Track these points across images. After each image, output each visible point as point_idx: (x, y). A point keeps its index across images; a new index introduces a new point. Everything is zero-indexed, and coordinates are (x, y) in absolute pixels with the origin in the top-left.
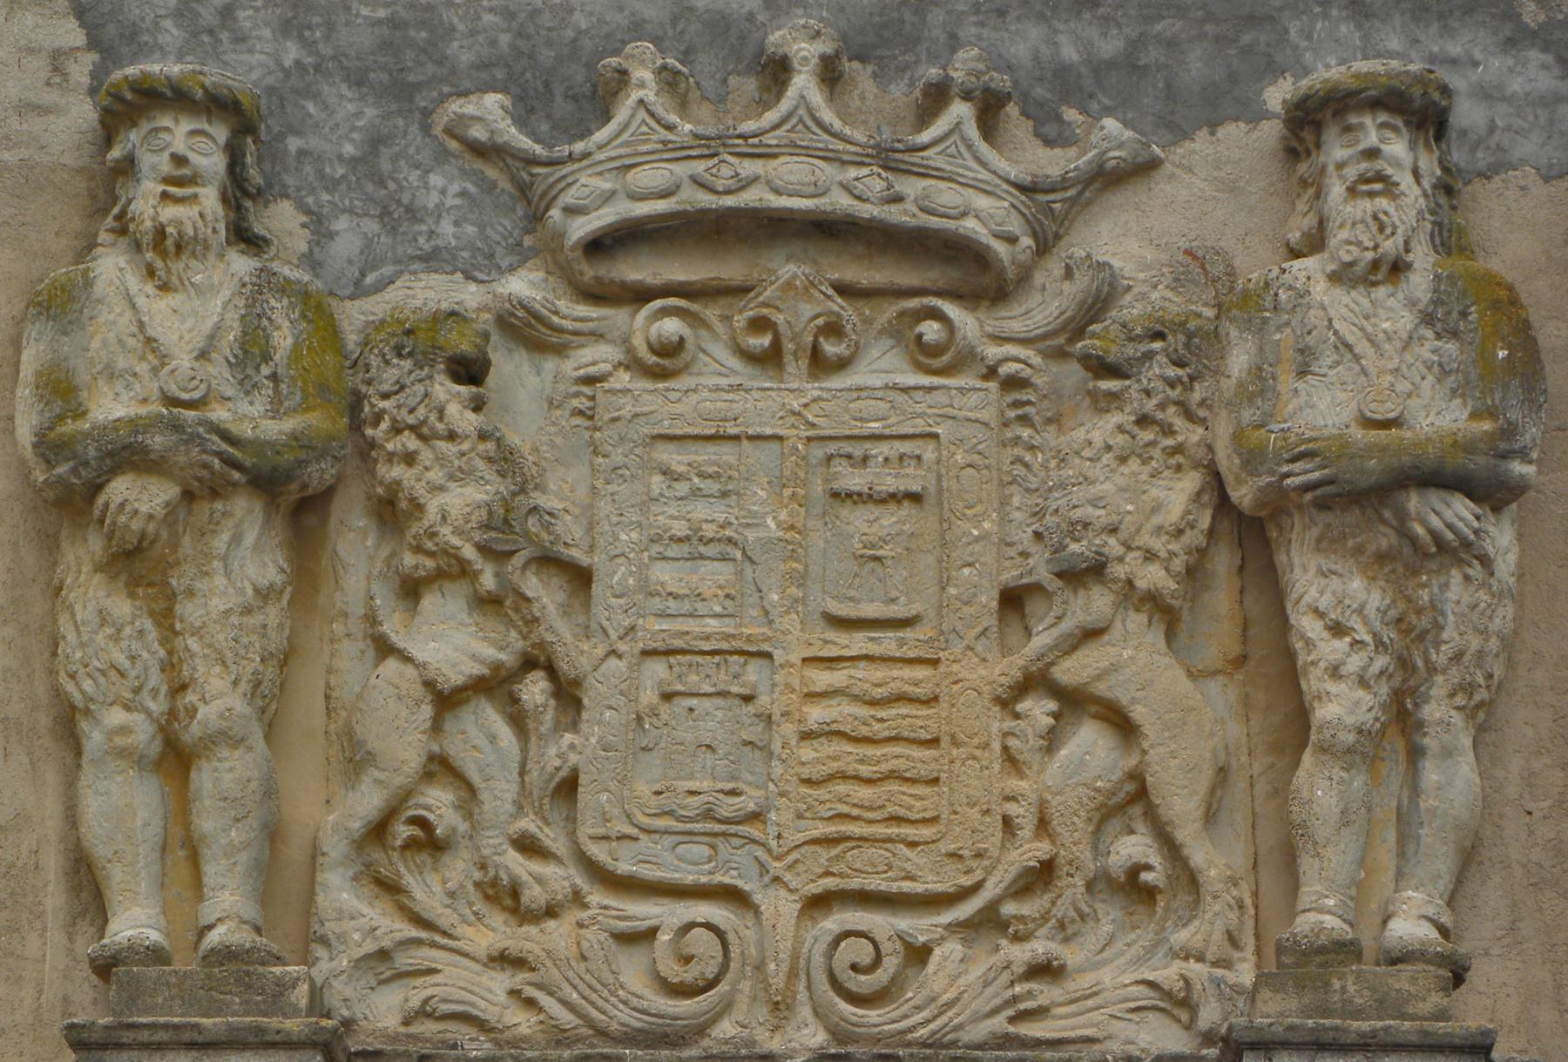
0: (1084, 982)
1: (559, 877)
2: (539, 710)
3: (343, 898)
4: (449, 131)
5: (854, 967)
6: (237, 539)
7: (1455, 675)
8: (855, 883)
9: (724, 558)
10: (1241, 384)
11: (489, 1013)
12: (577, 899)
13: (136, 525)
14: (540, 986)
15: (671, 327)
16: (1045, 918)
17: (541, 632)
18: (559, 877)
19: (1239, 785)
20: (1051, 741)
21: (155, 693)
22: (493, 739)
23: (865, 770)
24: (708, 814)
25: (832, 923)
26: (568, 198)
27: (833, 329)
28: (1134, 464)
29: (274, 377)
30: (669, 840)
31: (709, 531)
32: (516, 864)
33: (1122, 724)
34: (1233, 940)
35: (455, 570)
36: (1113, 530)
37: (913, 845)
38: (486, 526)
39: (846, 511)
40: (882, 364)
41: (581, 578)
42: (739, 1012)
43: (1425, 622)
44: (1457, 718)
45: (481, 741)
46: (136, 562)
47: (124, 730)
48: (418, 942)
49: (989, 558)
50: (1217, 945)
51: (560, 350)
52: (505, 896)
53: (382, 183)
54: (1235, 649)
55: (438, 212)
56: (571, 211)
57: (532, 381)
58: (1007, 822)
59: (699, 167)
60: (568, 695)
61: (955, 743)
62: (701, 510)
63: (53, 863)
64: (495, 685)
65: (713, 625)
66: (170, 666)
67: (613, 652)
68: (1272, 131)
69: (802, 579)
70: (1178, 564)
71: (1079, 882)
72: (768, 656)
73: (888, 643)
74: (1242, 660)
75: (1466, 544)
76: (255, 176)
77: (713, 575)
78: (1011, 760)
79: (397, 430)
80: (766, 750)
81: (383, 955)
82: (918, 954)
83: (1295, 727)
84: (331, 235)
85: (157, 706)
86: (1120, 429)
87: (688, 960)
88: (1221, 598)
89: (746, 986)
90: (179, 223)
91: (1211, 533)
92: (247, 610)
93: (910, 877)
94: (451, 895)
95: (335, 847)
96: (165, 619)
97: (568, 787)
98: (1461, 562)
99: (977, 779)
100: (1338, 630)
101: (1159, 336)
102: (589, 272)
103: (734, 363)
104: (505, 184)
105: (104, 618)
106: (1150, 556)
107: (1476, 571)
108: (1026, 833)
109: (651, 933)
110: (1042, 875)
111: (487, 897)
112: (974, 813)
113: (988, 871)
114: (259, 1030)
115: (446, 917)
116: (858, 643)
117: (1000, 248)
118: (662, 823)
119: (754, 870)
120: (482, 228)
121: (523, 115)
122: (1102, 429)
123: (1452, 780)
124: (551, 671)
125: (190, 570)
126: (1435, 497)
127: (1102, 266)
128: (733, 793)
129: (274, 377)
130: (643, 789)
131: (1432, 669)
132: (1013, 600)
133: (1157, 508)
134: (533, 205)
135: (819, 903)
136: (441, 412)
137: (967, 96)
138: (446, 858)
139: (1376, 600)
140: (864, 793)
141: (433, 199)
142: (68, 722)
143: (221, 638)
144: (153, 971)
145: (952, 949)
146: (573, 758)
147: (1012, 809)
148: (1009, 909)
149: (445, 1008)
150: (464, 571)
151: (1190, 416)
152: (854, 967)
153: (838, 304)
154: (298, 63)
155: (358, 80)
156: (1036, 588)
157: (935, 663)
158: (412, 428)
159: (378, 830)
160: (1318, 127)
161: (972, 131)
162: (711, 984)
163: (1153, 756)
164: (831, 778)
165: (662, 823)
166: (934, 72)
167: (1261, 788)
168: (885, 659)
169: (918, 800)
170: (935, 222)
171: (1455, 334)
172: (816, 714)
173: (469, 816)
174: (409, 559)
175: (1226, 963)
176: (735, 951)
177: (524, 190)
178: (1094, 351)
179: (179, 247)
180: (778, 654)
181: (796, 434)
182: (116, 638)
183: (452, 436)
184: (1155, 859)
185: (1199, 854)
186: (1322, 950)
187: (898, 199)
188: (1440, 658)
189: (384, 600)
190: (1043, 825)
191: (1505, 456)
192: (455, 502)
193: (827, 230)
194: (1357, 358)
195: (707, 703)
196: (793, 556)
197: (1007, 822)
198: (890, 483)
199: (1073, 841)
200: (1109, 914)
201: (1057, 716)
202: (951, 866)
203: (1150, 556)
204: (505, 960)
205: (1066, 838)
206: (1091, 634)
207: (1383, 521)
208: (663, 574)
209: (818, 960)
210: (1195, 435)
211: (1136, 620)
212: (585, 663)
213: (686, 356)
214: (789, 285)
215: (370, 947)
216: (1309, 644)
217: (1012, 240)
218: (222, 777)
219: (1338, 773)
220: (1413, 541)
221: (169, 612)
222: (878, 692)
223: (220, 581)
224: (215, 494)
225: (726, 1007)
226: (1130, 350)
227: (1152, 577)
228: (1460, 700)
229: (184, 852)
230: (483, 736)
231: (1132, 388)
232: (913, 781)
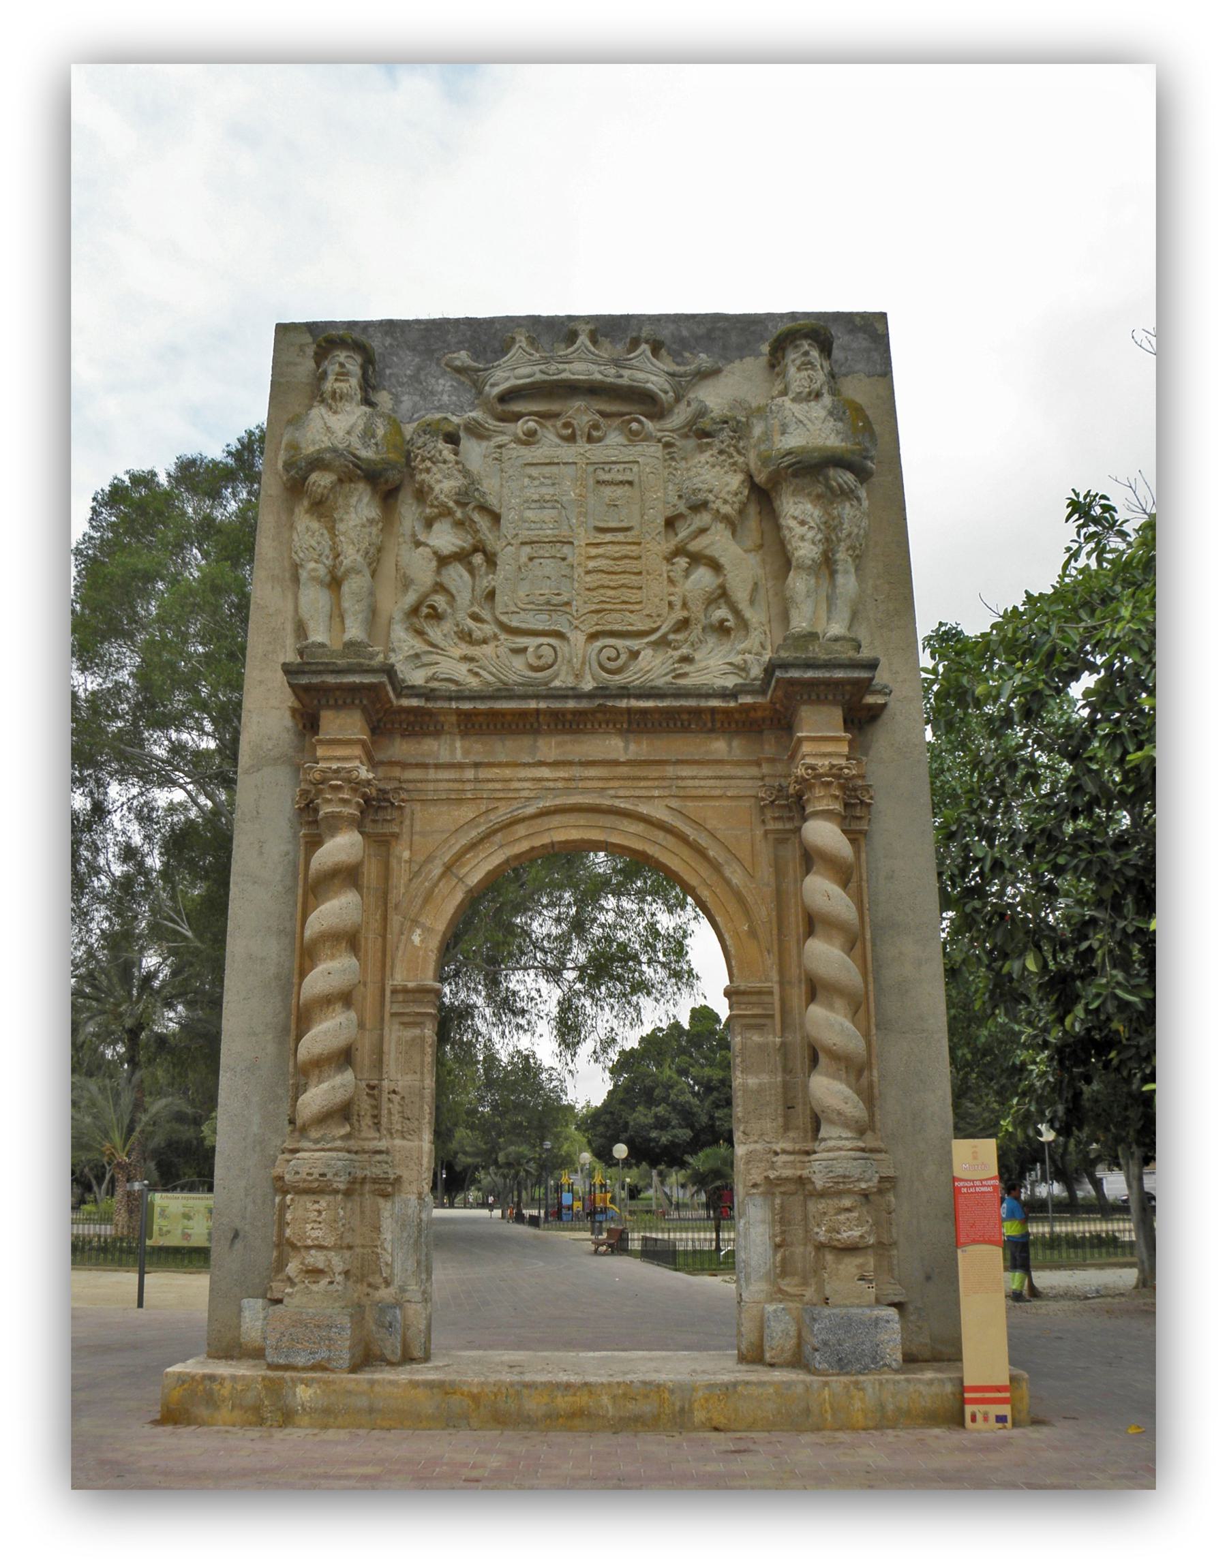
0: (703, 664)
1: (489, 629)
2: (480, 566)
3: (400, 634)
4: (447, 365)
5: (609, 659)
6: (360, 500)
7: (848, 542)
8: (608, 628)
9: (554, 508)
10: (759, 438)
11: (460, 678)
12: (496, 637)
13: (319, 490)
14: (480, 667)
15: (532, 424)
16: (686, 641)
17: (481, 535)
18: (489, 629)
19: (762, 591)
20: (687, 573)
21: (328, 558)
22: (461, 577)
23: (612, 584)
24: (548, 603)
25: (599, 644)
26: (492, 381)
27: (596, 427)
28: (718, 468)
29: (376, 444)
30: (532, 613)
31: (547, 497)
32: (471, 623)
33: (716, 567)
34: (763, 646)
35: (446, 513)
36: (711, 491)
37: (632, 612)
38: (457, 494)
39: (602, 488)
40: (615, 438)
41: (496, 518)
42: (561, 677)
43: (836, 522)
44: (849, 559)
45: (457, 578)
46: (321, 507)
47: (314, 570)
48: (431, 653)
49: (661, 506)
50: (756, 648)
51: (488, 438)
52: (467, 637)
53: (421, 383)
54: (759, 542)
55: (442, 393)
56: (493, 385)
57: (478, 449)
58: (670, 604)
59: (543, 367)
60: (491, 561)
61: (648, 573)
62: (544, 490)
63: (290, 627)
64: (462, 557)
65: (549, 532)
66: (333, 548)
67: (509, 544)
68: (763, 360)
69: (585, 514)
70: (736, 506)
71: (699, 627)
72: (572, 543)
73: (620, 537)
74: (761, 546)
75: (852, 491)
76: (373, 381)
77: (548, 514)
78: (671, 581)
79: (423, 461)
80: (571, 578)
81: (417, 656)
82: (634, 655)
83: (785, 562)
84: (401, 402)
85: (329, 562)
86: (712, 456)
87: (540, 657)
88: (753, 522)
89: (564, 668)
90: (341, 389)
91: (748, 498)
92: (363, 526)
93: (631, 625)
94: (445, 635)
95: (398, 616)
96: (332, 530)
97: (491, 595)
98: (849, 499)
99: (656, 588)
100: (803, 523)
101: (726, 422)
102: (499, 408)
103: (558, 441)
104: (467, 382)
105: (308, 529)
106: (725, 502)
107: (855, 503)
108: (678, 607)
109: (525, 650)
110: (684, 624)
111: (459, 638)
112: (657, 600)
113: (663, 622)
114: (361, 665)
115: (442, 644)
116: (608, 537)
117: (662, 395)
118: (529, 607)
119: (567, 624)
120: (459, 397)
121: (476, 356)
122: (705, 457)
123: (847, 583)
124: (485, 552)
125: (341, 511)
126: (840, 471)
127: (702, 401)
128: (558, 594)
129: (376, 444)
130: (521, 594)
131: (839, 540)
132: (670, 523)
133: (727, 485)
134: (478, 388)
135: (593, 637)
136: (441, 452)
137: (647, 342)
138: (443, 623)
139: (817, 513)
140: (611, 593)
141: (440, 388)
142: (296, 567)
143: (353, 535)
144: (321, 650)
145: (647, 654)
146: (493, 583)
147: (672, 598)
148: (671, 637)
149: (442, 676)
150: (449, 513)
151: (739, 452)
152: (609, 659)
153: (597, 417)
154: (391, 345)
155: (413, 349)
156: (681, 516)
157: (639, 544)
158: (429, 459)
159: (415, 611)
160: (784, 349)
161: (649, 353)
162: (551, 666)
163: (729, 576)
164: (598, 587)
165: (529, 607)
166: (634, 334)
167: (771, 593)
168: (619, 543)
169: (634, 596)
170: (635, 384)
171: (841, 420)
172: (591, 564)
173: (452, 607)
174: (428, 510)
175: (761, 655)
176: (560, 654)
177: (475, 383)
178: (700, 432)
179: (341, 398)
180: (576, 543)
181: (582, 462)
182: (312, 536)
183: (445, 462)
184: (730, 617)
185: (748, 613)
186: (804, 636)
187: (621, 376)
188: (842, 535)
189: (419, 528)
190: (685, 605)
191: (865, 458)
192: (445, 485)
193: (593, 390)
194: (805, 425)
195: (548, 561)
196: (581, 506)
197: (670, 604)
198: (620, 478)
199: (697, 610)
200: (712, 641)
201: (689, 564)
202: (648, 620)
203: (725, 502)
204: (466, 659)
205: (694, 609)
206: (703, 531)
207: (819, 481)
208: (529, 514)
209: (594, 656)
210: (741, 460)
211: (721, 526)
212: (498, 548)
213: (538, 437)
214: (578, 409)
215: (412, 652)
216: (790, 529)
217: (666, 392)
218: (351, 586)
219: (805, 576)
220: (830, 488)
221: (333, 528)
222: (617, 555)
223: (353, 516)
224: (351, 481)
225: (556, 676)
226: (715, 427)
227: (726, 509)
228: (850, 552)
229: (337, 616)
230: (456, 576)
231: (716, 441)
232: (632, 588)
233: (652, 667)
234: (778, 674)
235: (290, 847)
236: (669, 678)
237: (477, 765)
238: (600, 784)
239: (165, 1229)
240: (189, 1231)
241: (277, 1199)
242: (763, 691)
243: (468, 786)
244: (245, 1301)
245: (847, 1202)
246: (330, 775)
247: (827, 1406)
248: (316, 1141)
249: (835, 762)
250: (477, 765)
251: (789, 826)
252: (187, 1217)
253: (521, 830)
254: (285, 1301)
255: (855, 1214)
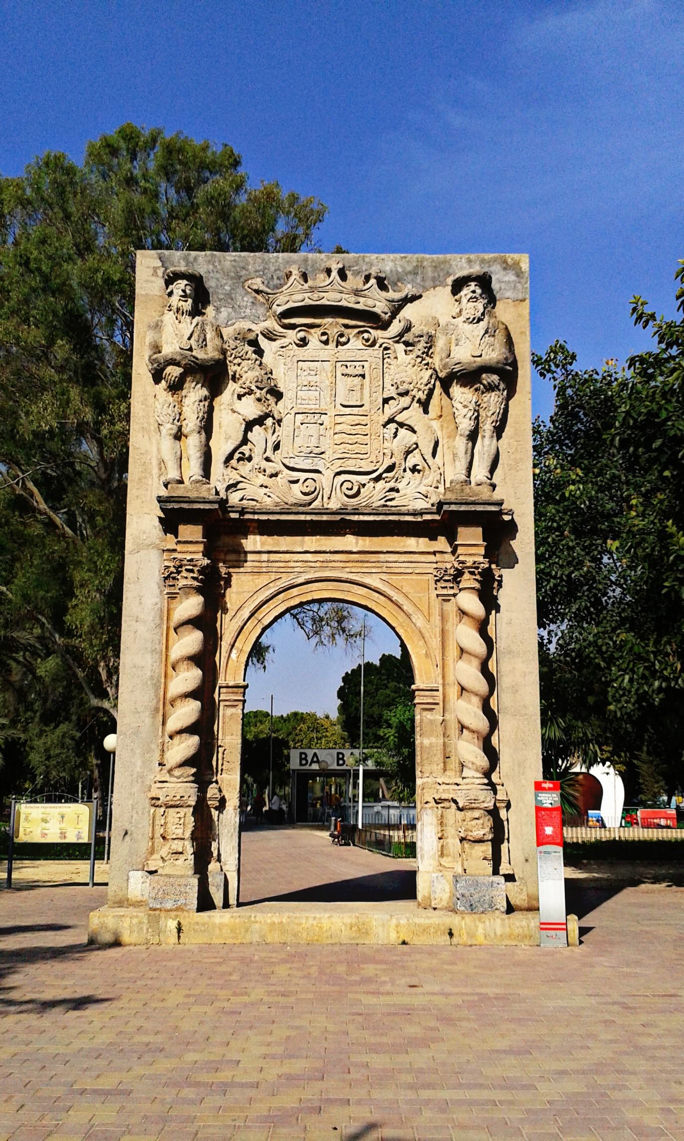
27: (342, 335)
31: (312, 384)
62: (310, 378)
65: (313, 406)
70: (426, 392)
79: (235, 358)
92: (201, 401)
106: (419, 390)
110: (391, 468)
117: (383, 315)
153: (343, 329)
172: (338, 428)
175: (437, 488)
233: (374, 494)
234: (445, 507)
235: (158, 600)
236: (382, 502)
237: (269, 552)
238: (342, 565)
239: (28, 830)
240: (46, 831)
241: (152, 811)
242: (438, 513)
243: (264, 564)
244: (131, 873)
245: (477, 814)
246: (185, 562)
247: (464, 931)
248: (178, 778)
249: (476, 560)
250: (269, 552)
251: (451, 592)
252: (45, 821)
253: (295, 591)
254: (159, 872)
255: (481, 821)
